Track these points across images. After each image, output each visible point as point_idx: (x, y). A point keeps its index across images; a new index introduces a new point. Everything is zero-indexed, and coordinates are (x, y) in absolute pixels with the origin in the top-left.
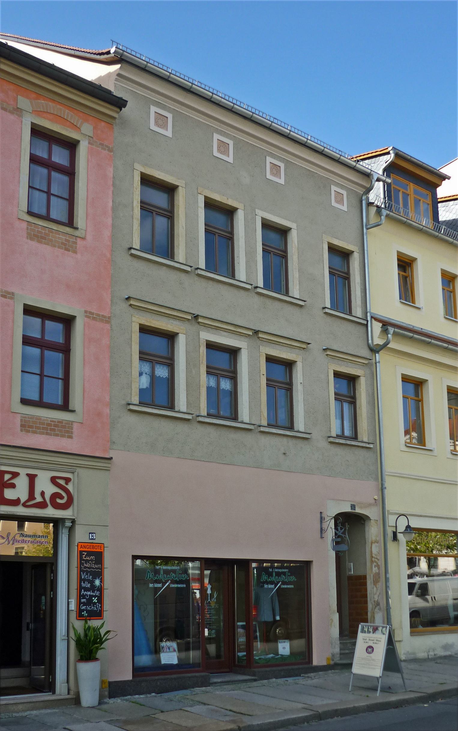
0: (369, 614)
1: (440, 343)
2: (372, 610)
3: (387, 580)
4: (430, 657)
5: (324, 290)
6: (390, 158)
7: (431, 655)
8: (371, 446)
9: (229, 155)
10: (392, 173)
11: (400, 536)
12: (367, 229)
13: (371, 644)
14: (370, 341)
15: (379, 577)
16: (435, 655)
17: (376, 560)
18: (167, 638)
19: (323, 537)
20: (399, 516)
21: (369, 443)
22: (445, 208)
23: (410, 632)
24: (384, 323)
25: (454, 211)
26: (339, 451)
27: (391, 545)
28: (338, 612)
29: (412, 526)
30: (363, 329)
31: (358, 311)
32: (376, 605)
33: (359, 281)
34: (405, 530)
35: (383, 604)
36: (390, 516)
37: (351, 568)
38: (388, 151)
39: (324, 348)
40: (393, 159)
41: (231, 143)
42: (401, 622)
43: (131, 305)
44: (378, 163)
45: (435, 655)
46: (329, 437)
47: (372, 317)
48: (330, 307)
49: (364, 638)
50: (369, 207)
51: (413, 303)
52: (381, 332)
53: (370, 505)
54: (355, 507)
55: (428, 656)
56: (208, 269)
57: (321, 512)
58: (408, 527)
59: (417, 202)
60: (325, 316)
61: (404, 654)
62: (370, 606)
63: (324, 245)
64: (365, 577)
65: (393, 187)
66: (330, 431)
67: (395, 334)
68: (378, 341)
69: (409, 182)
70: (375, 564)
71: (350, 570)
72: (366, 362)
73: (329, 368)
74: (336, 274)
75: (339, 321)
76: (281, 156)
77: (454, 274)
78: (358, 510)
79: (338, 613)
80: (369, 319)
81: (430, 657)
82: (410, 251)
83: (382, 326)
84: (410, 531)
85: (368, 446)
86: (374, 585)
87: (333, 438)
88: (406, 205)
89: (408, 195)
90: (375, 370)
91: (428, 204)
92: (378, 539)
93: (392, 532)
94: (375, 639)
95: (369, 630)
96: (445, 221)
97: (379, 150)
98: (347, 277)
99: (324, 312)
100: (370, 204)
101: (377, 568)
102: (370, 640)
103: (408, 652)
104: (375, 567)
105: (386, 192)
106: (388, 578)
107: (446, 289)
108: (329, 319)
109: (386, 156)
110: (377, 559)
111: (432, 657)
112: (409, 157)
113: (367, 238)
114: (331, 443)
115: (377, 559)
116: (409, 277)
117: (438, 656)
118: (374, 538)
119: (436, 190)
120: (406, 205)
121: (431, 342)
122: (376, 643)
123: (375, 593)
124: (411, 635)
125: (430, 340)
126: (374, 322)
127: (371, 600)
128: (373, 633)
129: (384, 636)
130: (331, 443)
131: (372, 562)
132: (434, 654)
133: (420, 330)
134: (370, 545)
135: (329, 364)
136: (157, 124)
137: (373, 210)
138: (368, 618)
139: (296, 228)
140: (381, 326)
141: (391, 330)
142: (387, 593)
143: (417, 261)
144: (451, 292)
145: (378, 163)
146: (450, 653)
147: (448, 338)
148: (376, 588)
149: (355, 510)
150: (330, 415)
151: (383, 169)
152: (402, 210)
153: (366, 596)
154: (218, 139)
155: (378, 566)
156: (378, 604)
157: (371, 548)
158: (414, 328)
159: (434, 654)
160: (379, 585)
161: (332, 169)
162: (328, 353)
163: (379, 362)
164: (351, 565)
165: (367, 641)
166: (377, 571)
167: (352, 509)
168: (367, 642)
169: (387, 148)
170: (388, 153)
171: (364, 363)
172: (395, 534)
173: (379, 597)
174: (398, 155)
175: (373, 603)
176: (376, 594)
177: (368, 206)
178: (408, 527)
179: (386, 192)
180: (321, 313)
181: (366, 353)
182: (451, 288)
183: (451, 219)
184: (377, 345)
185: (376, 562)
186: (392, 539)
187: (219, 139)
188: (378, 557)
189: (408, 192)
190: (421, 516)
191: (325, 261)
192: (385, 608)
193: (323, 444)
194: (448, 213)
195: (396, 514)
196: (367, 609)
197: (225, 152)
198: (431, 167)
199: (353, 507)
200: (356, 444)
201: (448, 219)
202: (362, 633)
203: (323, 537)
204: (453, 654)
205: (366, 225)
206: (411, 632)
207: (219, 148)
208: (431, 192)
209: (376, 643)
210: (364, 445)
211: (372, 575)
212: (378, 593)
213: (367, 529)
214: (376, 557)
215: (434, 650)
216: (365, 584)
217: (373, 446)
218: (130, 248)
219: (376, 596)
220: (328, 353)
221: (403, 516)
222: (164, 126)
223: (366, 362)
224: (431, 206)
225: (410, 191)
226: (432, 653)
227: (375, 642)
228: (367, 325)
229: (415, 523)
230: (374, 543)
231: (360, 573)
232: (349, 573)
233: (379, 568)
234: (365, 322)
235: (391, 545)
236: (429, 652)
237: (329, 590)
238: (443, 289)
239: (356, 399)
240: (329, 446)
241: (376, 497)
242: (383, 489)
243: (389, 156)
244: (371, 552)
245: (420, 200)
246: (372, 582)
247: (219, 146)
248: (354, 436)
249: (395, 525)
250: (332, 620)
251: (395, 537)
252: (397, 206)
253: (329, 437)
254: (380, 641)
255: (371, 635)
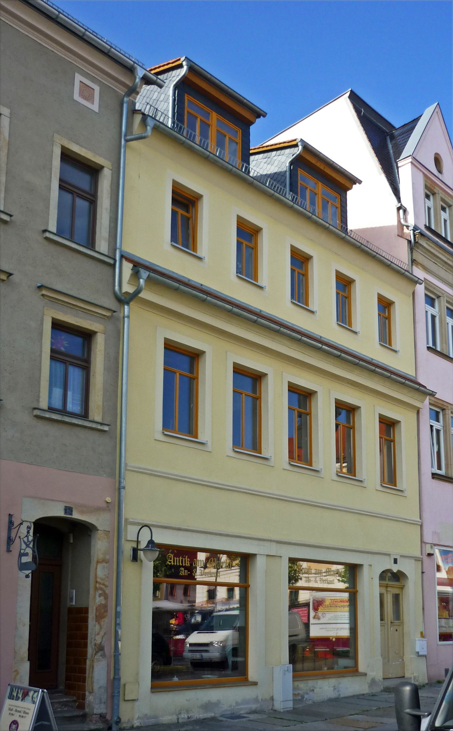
0: (88, 662)
1: (289, 332)
2: (92, 656)
3: (118, 615)
4: (180, 721)
5: (48, 207)
6: (183, 71)
7: (183, 718)
8: (106, 428)
9: (93, 101)
10: (300, 168)
11: (141, 554)
12: (127, 141)
13: (16, 718)
14: (117, 288)
15: (106, 611)
16: (189, 718)
17: (102, 586)
18: (155, 662)
19: (11, 551)
20: (141, 526)
21: (102, 424)
22: (267, 159)
23: (150, 687)
24: (135, 264)
25: (276, 164)
26: (53, 431)
27: (129, 568)
28: (29, 660)
29: (156, 542)
30: (107, 270)
31: (102, 245)
32: (97, 650)
33: (109, 207)
34: (146, 547)
35: (109, 649)
36: (130, 527)
37: (73, 596)
38: (181, 62)
39: (39, 285)
40: (300, 152)
41: (97, 88)
42: (138, 674)
43: (43, 295)
44: (170, 79)
45: (189, 718)
46: (35, 409)
47: (122, 257)
48: (55, 232)
49: (10, 707)
50: (135, 115)
51: (194, 251)
52: (131, 276)
53: (97, 510)
54: (72, 511)
55: (178, 719)
56: (59, 233)
57: (10, 514)
58: (151, 542)
59: (325, 204)
60: (46, 243)
61: (139, 718)
62: (90, 650)
63: (54, 147)
64: (86, 610)
65: (300, 183)
66: (38, 401)
67: (149, 279)
68: (127, 288)
69: (211, 111)
70: (100, 592)
71: (71, 599)
72: (108, 314)
73: (45, 313)
74: (74, 192)
75: (69, 254)
76: (37, 40)
77: (390, 300)
78: (76, 516)
79: (29, 662)
80: (118, 258)
81: (180, 721)
82: (305, 247)
83: (133, 267)
84: (151, 547)
85: (99, 427)
86: (96, 621)
87: (40, 411)
88: (313, 203)
89: (316, 194)
90: (121, 326)
91: (337, 208)
92: (107, 557)
93: (132, 549)
94: (22, 709)
95: (19, 695)
96: (266, 174)
97: (171, 61)
98: (92, 200)
99: (45, 236)
100: (134, 111)
101: (102, 598)
102: (16, 711)
103: (146, 715)
104: (100, 596)
105: (176, 114)
106: (120, 612)
107: (341, 293)
108: (52, 248)
109: (292, 149)
110: (103, 584)
111: (184, 721)
112: (209, 76)
113: (125, 152)
114: (37, 417)
115: (103, 584)
116: (192, 218)
117: (193, 719)
118: (101, 556)
119: (249, 128)
120: (313, 203)
121: (358, 363)
122: (22, 717)
123: (96, 633)
124: (152, 692)
125: (206, 296)
126: (125, 263)
127: (91, 642)
128: (22, 700)
129: (34, 705)
130: (37, 417)
131: (96, 589)
132: (188, 716)
133: (200, 286)
134: (95, 565)
135: (45, 308)
136: (81, 95)
137: (138, 118)
138: (86, 667)
139: (9, 115)
140: (131, 268)
141: (144, 274)
142: (116, 632)
143: (395, 305)
144: (387, 319)
145: (170, 79)
146: (213, 715)
147: (280, 320)
148: (100, 626)
149: (71, 514)
150: (40, 378)
151: (174, 85)
152: (197, 140)
153: (85, 637)
154: (81, 81)
155: (105, 596)
156: (100, 648)
157: (96, 569)
158: (190, 282)
159: (188, 716)
160: (105, 622)
161: (29, 20)
162: (44, 292)
163: (128, 317)
164: (73, 593)
165: (13, 712)
166: (103, 602)
167: (66, 513)
168: (12, 714)
169: (179, 60)
170: (180, 66)
171: (104, 315)
172: (135, 551)
173: (104, 639)
174: (192, 69)
175: (94, 647)
176: (98, 634)
177: (134, 113)
178: (151, 542)
179: (176, 114)
180: (40, 239)
181: (111, 303)
182: (387, 314)
183: (273, 172)
184: (127, 293)
185: (101, 589)
186: (132, 558)
187: (81, 80)
188: (106, 583)
189: (316, 191)
190: (179, 529)
191: (53, 169)
192: (112, 653)
193: (25, 418)
194: (269, 166)
195: (138, 524)
196: (86, 655)
197: (90, 97)
198: (239, 94)
199: (68, 510)
200: (80, 423)
201: (269, 173)
202: (10, 699)
203: (11, 550)
204: (218, 715)
205: (125, 135)
206: (152, 687)
207: (82, 94)
208: (242, 130)
209: (22, 717)
210: (94, 426)
211: (95, 608)
212: (102, 633)
213: (93, 543)
214: (102, 582)
215: (187, 711)
216: (86, 620)
217: (109, 429)
218: (45, 231)
219: (98, 637)
220: (44, 292)
221: (146, 527)
222: (89, 98)
223: (108, 314)
224: (340, 210)
225: (212, 122)
226: (184, 716)
227: (22, 714)
228: (114, 266)
229: (161, 538)
230: (101, 562)
231: (82, 605)
232: (71, 604)
233: (106, 598)
234: (112, 262)
235: (129, 568)
236: (180, 713)
237: (16, 628)
238: (379, 315)
239: (90, 362)
240: (35, 422)
241: (108, 499)
242: (120, 488)
243: (297, 148)
244: (96, 575)
245: (328, 202)
246: (95, 617)
247: (82, 91)
248: (83, 414)
249: (136, 540)
250: (17, 672)
251: (135, 558)
252: (191, 133)
253: (35, 409)
254: (28, 714)
255: (19, 703)
